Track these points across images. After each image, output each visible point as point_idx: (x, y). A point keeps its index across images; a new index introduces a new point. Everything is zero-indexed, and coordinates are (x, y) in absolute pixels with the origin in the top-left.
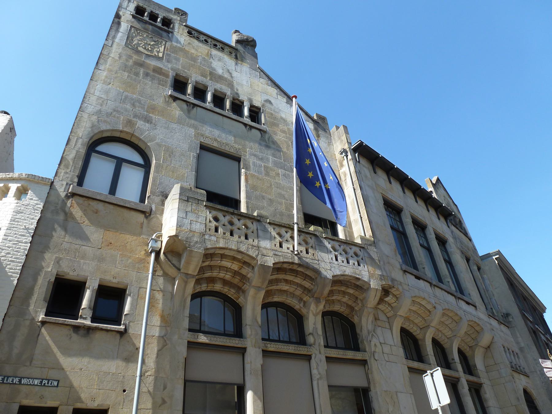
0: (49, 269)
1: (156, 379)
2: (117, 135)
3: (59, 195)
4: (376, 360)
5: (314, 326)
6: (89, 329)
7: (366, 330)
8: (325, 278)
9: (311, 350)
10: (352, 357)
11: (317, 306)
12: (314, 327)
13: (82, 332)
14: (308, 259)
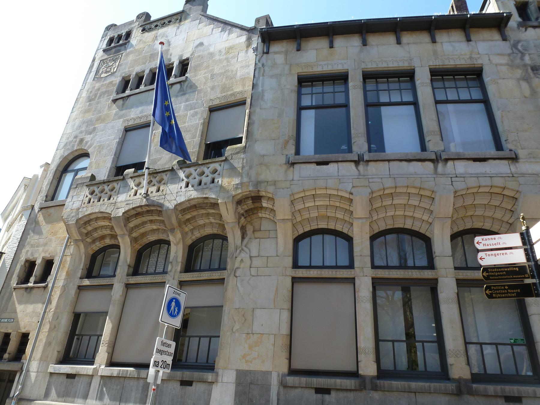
0: (22, 259)
1: (54, 314)
2: (77, 154)
3: (35, 212)
4: (236, 277)
5: (175, 255)
6: (32, 288)
7: (234, 247)
8: (168, 209)
9: (166, 277)
10: (207, 277)
11: (174, 236)
12: (175, 256)
13: (28, 290)
14: (156, 197)
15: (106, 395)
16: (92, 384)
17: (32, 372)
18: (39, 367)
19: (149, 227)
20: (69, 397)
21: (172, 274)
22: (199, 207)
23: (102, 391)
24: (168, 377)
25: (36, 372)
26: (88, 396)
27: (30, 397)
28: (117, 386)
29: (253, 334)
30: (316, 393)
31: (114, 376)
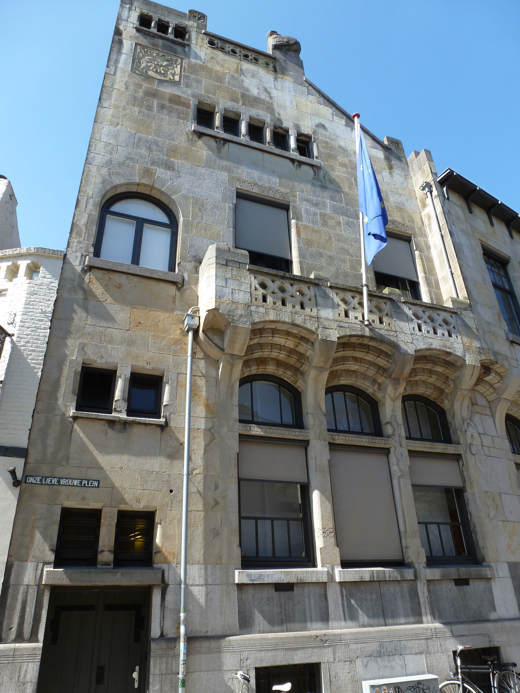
1: (205, 478)
4: (473, 455)
8: (406, 353)
10: (441, 450)
11: (395, 389)
13: (117, 427)
15: (359, 610)
16: (328, 597)
17: (192, 586)
18: (206, 575)
19: (354, 366)
20: (294, 621)
21: (396, 438)
22: (431, 361)
23: (350, 606)
24: (441, 576)
25: (202, 585)
26: (328, 615)
27: (207, 632)
28: (371, 595)
29: (508, 521)
30: (455, 585)
31: (365, 581)
